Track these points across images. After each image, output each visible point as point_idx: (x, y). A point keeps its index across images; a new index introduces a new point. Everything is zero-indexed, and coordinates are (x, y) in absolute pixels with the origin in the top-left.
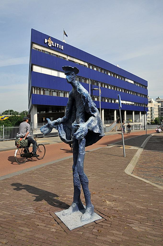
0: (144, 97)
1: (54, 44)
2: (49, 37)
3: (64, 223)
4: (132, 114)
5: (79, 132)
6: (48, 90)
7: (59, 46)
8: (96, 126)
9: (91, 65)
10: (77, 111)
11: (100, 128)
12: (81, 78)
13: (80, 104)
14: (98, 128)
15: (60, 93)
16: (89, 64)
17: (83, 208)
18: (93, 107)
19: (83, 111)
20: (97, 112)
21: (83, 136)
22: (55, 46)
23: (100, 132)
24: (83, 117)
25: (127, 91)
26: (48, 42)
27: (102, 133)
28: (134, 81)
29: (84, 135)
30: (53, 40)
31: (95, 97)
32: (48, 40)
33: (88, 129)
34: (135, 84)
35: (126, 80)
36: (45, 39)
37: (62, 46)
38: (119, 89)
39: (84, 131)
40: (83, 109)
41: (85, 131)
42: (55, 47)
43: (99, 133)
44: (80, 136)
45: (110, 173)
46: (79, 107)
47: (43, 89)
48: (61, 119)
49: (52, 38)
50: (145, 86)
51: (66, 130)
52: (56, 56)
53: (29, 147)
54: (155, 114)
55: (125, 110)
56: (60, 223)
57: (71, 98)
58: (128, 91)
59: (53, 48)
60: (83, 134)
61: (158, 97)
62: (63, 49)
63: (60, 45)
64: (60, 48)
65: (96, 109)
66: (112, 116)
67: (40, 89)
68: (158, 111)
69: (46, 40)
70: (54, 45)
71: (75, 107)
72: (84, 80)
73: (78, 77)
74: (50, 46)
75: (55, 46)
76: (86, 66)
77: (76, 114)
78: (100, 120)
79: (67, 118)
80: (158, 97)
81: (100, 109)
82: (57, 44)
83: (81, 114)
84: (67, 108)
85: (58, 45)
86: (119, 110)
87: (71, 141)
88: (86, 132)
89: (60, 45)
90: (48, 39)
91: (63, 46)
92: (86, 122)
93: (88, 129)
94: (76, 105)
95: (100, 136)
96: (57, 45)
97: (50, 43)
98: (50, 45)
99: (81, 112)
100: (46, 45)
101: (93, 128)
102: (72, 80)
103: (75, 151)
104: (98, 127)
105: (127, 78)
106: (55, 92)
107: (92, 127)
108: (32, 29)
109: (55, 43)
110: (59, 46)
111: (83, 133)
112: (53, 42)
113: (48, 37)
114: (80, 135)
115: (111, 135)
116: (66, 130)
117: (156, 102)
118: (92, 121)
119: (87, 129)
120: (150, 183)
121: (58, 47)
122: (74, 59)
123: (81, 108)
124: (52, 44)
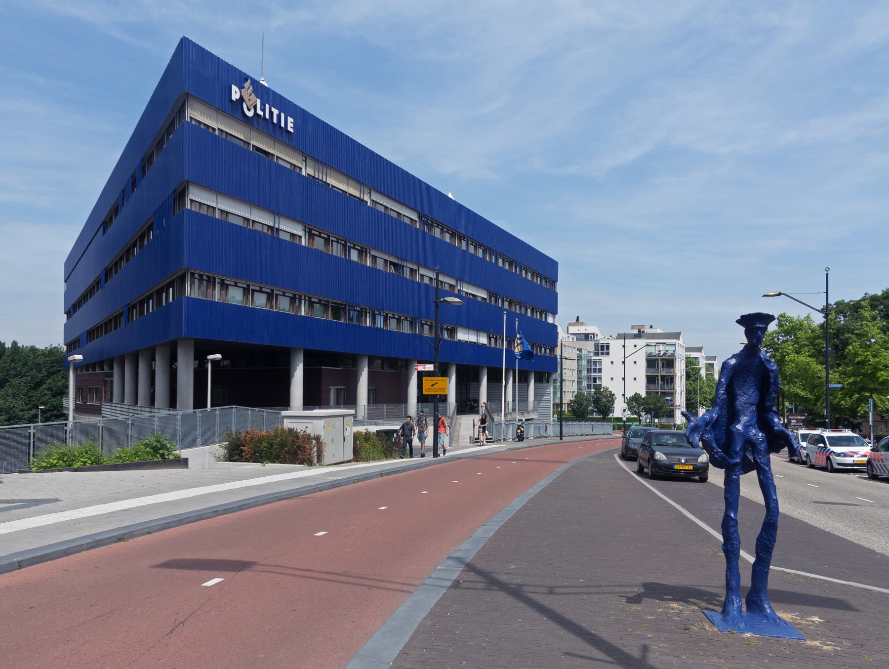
1: (263, 110)
2: (246, 80)
4: (478, 381)
6: (238, 284)
7: (279, 117)
12: (349, 244)
15: (279, 296)
22: (267, 116)
26: (241, 100)
30: (264, 93)
31: (390, 317)
32: (243, 90)
36: (233, 86)
37: (290, 120)
42: (265, 118)
47: (310, 298)
49: (255, 84)
52: (288, 166)
56: (645, 589)
59: (258, 123)
61: (578, 318)
62: (292, 130)
63: (283, 115)
64: (283, 125)
67: (211, 281)
69: (234, 88)
70: (261, 113)
72: (323, 240)
73: (338, 239)
74: (250, 114)
75: (267, 116)
76: (366, 202)
80: (578, 318)
81: (515, 370)
82: (273, 109)
85: (276, 112)
86: (795, 412)
89: (283, 115)
90: (241, 87)
91: (292, 120)
96: (271, 113)
97: (249, 103)
98: (249, 110)
100: (235, 110)
106: (284, 295)
109: (267, 106)
110: (279, 117)
112: (258, 101)
113: (242, 79)
115: (598, 439)
117: (571, 337)
120: (271, 569)
121: (275, 121)
124: (255, 107)
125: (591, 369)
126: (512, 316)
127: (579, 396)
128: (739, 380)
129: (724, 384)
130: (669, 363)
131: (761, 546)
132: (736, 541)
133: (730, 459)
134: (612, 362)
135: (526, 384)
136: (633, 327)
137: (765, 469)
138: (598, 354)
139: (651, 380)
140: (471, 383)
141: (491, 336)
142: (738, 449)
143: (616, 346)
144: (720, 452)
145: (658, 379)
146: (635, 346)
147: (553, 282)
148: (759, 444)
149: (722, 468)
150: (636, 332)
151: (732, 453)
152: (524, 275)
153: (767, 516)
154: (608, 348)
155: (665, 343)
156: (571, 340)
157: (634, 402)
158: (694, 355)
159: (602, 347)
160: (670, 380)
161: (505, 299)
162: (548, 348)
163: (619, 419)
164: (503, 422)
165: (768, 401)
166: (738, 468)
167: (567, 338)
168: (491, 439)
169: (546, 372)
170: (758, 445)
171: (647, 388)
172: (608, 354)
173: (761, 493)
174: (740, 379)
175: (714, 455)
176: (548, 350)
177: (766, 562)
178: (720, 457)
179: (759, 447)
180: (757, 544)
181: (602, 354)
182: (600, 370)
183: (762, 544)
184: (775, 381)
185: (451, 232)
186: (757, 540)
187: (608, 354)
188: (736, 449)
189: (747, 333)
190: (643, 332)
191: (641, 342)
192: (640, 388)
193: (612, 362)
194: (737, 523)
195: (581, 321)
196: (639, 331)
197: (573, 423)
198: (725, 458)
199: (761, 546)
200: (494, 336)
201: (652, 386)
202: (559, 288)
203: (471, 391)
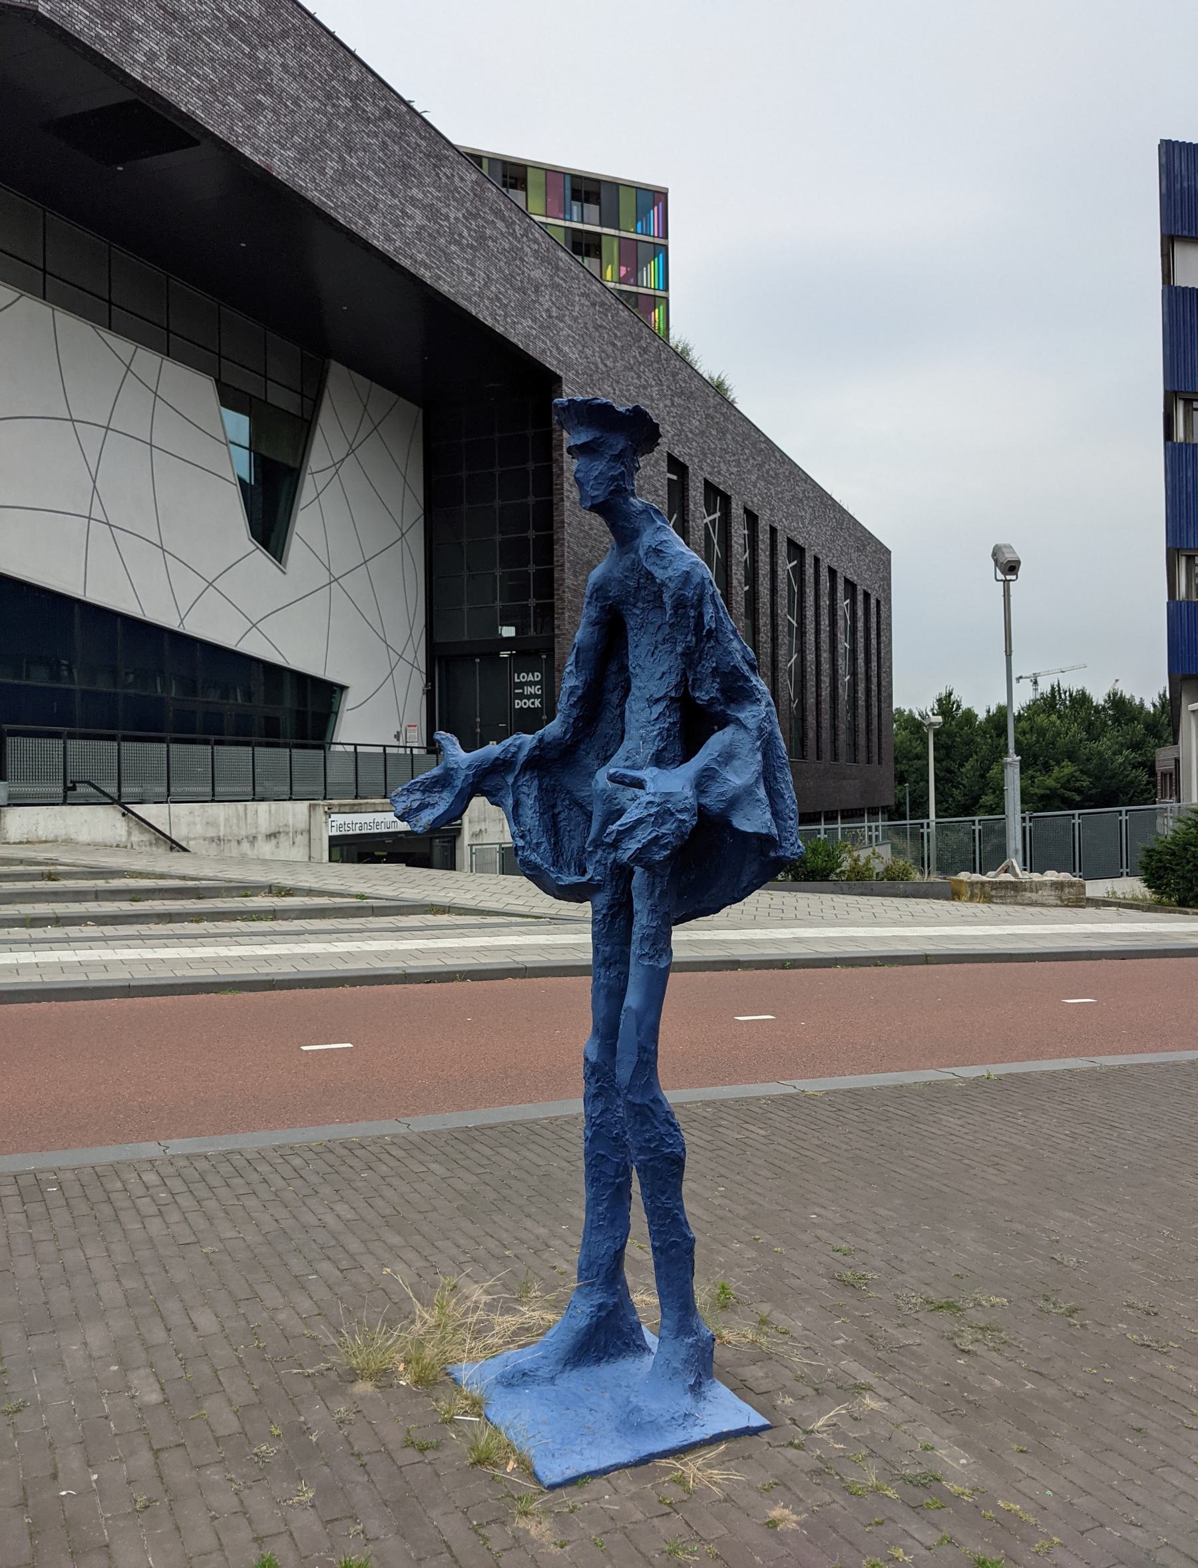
5: (639, 822)
8: (748, 791)
10: (633, 690)
11: (773, 804)
13: (656, 648)
14: (766, 800)
17: (638, 1346)
18: (735, 667)
19: (673, 695)
20: (764, 703)
21: (664, 847)
23: (775, 831)
24: (668, 730)
27: (786, 839)
29: (671, 839)
33: (700, 806)
39: (672, 814)
40: (673, 679)
41: (680, 816)
43: (767, 835)
44: (644, 847)
45: (603, 363)
46: (648, 664)
48: (529, 737)
51: (556, 811)
53: (549, 381)
57: (601, 608)
60: (664, 834)
65: (761, 684)
71: (624, 668)
77: (623, 713)
78: (779, 757)
79: (565, 733)
83: (659, 708)
84: (571, 671)
87: (584, 879)
88: (684, 821)
92: (686, 758)
93: (700, 806)
94: (627, 654)
95: (772, 854)
99: (658, 701)
101: (733, 803)
102: (611, 492)
103: (608, 948)
104: (762, 793)
107: (722, 794)
111: (663, 830)
114: (643, 836)
116: (556, 811)
118: (728, 757)
119: (691, 801)
122: (863, 655)
123: (658, 675)
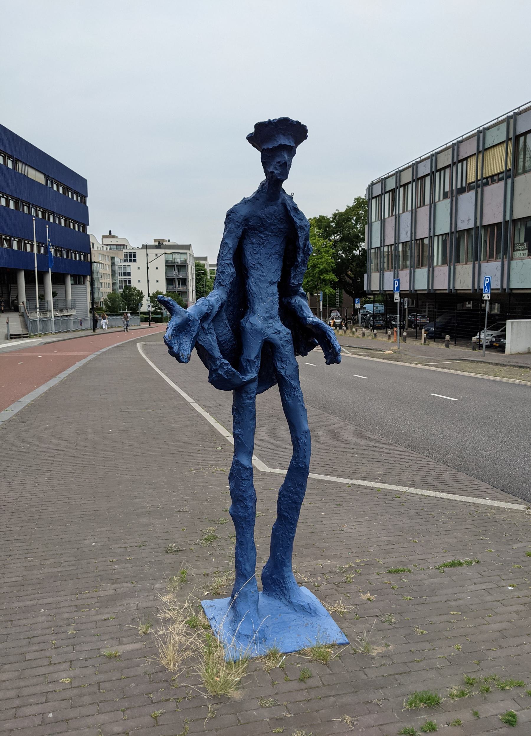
0: (77, 229)
3: (410, 228)
4: (15, 282)
9: (10, 157)
16: (47, 178)
25: (23, 206)
28: (45, 175)
34: (50, 185)
35: (20, 167)
38: (78, 225)
50: (80, 194)
54: (101, 283)
55: (20, 270)
58: (29, 204)
61: (110, 232)
66: (54, 300)
68: (111, 274)
80: (110, 232)
105: (23, 163)
108: (190, 245)
117: (105, 247)
125: (122, 273)
126: (42, 224)
127: (112, 297)
128: (253, 244)
129: (230, 249)
130: (183, 266)
131: (285, 502)
132: (250, 502)
133: (242, 375)
134: (139, 268)
135: (64, 286)
136: (155, 241)
137: (291, 385)
138: (127, 261)
139: (170, 281)
140: (12, 285)
141: (26, 242)
142: (253, 357)
143: (141, 256)
144: (227, 365)
145: (175, 281)
146: (156, 255)
147: (84, 197)
148: (282, 345)
149: (229, 390)
150: (157, 244)
151: (244, 364)
152: (55, 189)
153: (294, 457)
154: (135, 256)
155: (179, 253)
156: (105, 249)
157: (155, 299)
158: (202, 262)
159: (130, 255)
160: (184, 282)
161: (38, 209)
162: (82, 255)
163: (145, 313)
164: (38, 319)
165: (294, 278)
166: (254, 386)
167: (101, 247)
168: (27, 334)
169: (81, 275)
170: (282, 348)
171: (167, 288)
172: (135, 261)
173: (287, 422)
174: (254, 241)
175: (217, 370)
176: (82, 256)
177: (292, 524)
178: (227, 373)
179: (284, 352)
180: (279, 499)
181: (131, 261)
182: (129, 274)
183: (286, 499)
184: (305, 245)
185: (3, 155)
186: (280, 493)
187: (135, 261)
188: (250, 356)
189: (266, 162)
190: (162, 244)
191: (160, 251)
192: (162, 287)
193: (139, 268)
194: (252, 474)
195: (112, 234)
196: (159, 243)
197: (135, 317)
198: (234, 374)
199: (285, 502)
200: (43, 245)
201: (171, 287)
202: (89, 202)
203: (12, 292)
